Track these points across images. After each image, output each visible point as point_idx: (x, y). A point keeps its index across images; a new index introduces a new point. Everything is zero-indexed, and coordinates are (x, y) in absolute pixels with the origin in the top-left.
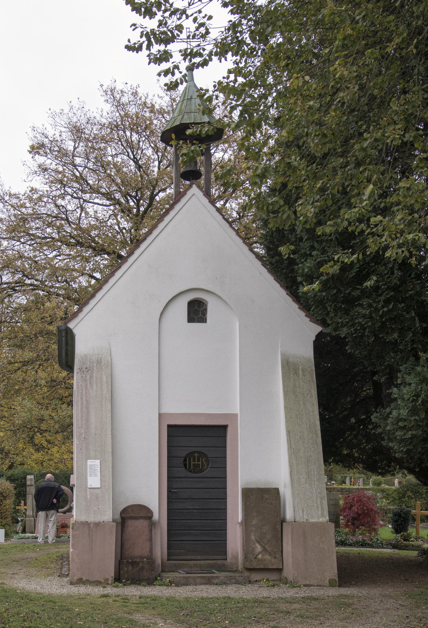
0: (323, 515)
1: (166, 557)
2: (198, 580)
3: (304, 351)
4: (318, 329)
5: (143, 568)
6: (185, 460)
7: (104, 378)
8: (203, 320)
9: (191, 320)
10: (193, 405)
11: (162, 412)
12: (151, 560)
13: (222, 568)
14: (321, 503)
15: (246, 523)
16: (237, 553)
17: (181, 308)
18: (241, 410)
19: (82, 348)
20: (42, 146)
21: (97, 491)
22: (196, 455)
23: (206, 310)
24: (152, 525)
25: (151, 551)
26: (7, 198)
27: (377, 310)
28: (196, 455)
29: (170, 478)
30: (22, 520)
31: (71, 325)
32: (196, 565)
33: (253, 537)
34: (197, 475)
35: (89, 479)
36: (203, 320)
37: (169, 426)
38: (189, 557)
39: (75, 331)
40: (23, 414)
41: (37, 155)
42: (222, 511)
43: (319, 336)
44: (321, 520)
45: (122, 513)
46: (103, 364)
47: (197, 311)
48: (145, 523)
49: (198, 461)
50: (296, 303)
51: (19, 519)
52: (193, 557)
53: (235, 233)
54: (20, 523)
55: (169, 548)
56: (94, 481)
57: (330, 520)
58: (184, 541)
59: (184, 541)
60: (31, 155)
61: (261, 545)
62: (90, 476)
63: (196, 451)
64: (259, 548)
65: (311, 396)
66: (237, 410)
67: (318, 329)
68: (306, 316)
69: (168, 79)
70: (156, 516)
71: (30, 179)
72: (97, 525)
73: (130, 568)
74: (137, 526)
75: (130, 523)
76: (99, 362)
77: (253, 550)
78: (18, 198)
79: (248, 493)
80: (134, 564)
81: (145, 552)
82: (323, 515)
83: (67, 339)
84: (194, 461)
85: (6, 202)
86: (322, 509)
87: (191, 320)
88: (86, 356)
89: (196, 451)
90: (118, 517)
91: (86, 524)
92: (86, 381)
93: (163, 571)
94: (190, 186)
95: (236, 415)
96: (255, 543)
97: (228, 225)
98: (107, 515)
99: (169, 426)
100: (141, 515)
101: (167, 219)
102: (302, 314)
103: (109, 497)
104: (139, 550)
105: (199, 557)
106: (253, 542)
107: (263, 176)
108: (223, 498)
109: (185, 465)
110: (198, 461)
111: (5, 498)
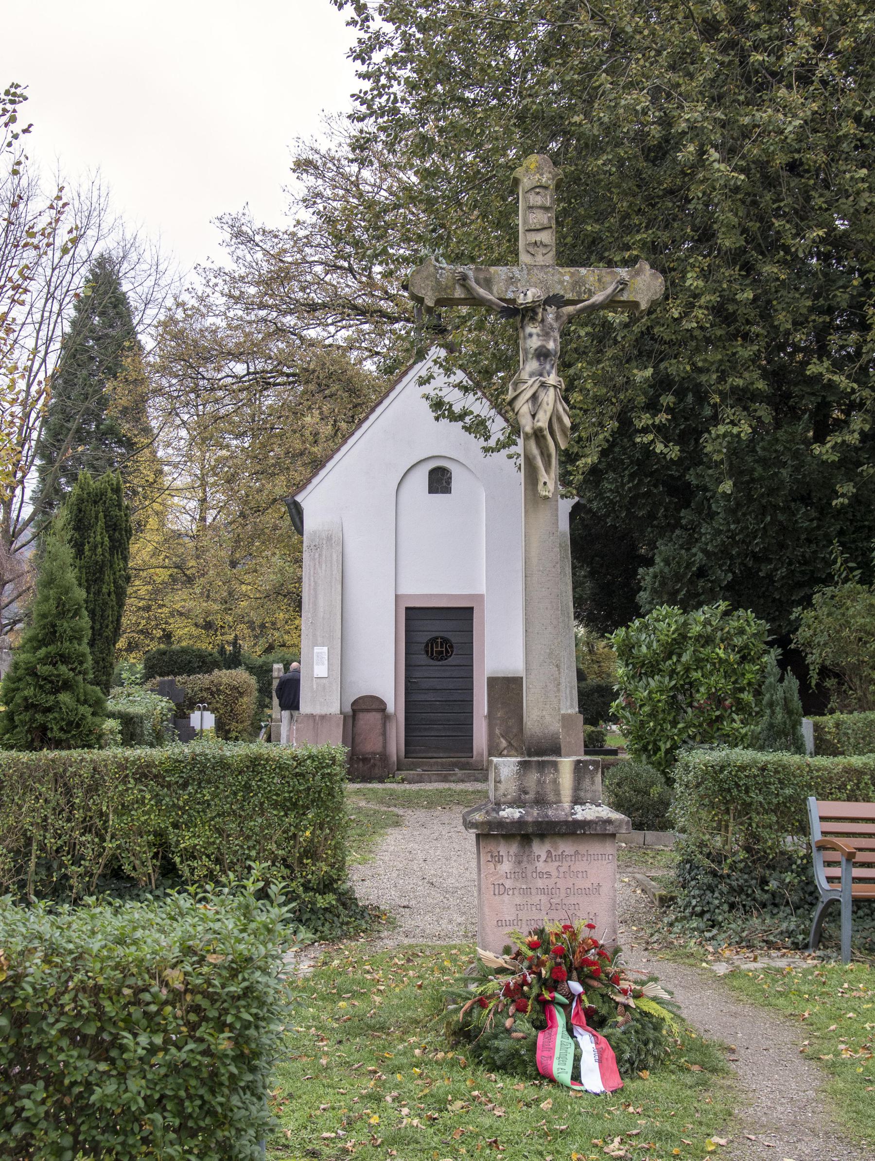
0: (572, 706)
1: (402, 753)
2: (434, 778)
5: (374, 765)
6: (427, 646)
7: (335, 556)
8: (447, 490)
9: (432, 490)
10: (434, 586)
11: (399, 593)
12: (384, 757)
13: (463, 767)
14: (571, 693)
15: (490, 716)
17: (421, 478)
18: (487, 590)
19: (310, 523)
20: (309, 163)
21: (324, 681)
23: (450, 478)
24: (386, 718)
25: (385, 746)
26: (258, 238)
27: (623, 485)
29: (408, 666)
30: (266, 726)
31: (298, 498)
32: (437, 763)
33: (497, 731)
34: (440, 663)
35: (315, 667)
36: (447, 490)
37: (407, 608)
38: (430, 755)
39: (303, 505)
40: (272, 577)
41: (305, 175)
42: (468, 702)
44: (569, 711)
45: (353, 704)
46: (335, 541)
47: (440, 480)
48: (378, 716)
51: (263, 724)
52: (435, 755)
54: (263, 730)
55: (406, 745)
56: (320, 670)
57: (580, 712)
60: (296, 175)
62: (317, 665)
63: (438, 637)
65: (565, 575)
66: (482, 589)
70: (391, 708)
71: (294, 210)
72: (323, 717)
73: (361, 764)
74: (369, 719)
75: (361, 715)
76: (329, 539)
77: (498, 745)
78: (276, 236)
79: (493, 682)
80: (365, 760)
81: (378, 748)
82: (572, 706)
83: (296, 512)
85: (257, 245)
86: (572, 699)
87: (432, 490)
88: (315, 532)
89: (438, 637)
90: (348, 709)
91: (312, 716)
92: (314, 559)
93: (398, 769)
95: (482, 596)
98: (334, 708)
99: (407, 608)
100: (373, 707)
101: (379, 410)
103: (336, 687)
104: (371, 745)
105: (441, 755)
108: (469, 690)
109: (427, 652)
111: (241, 694)
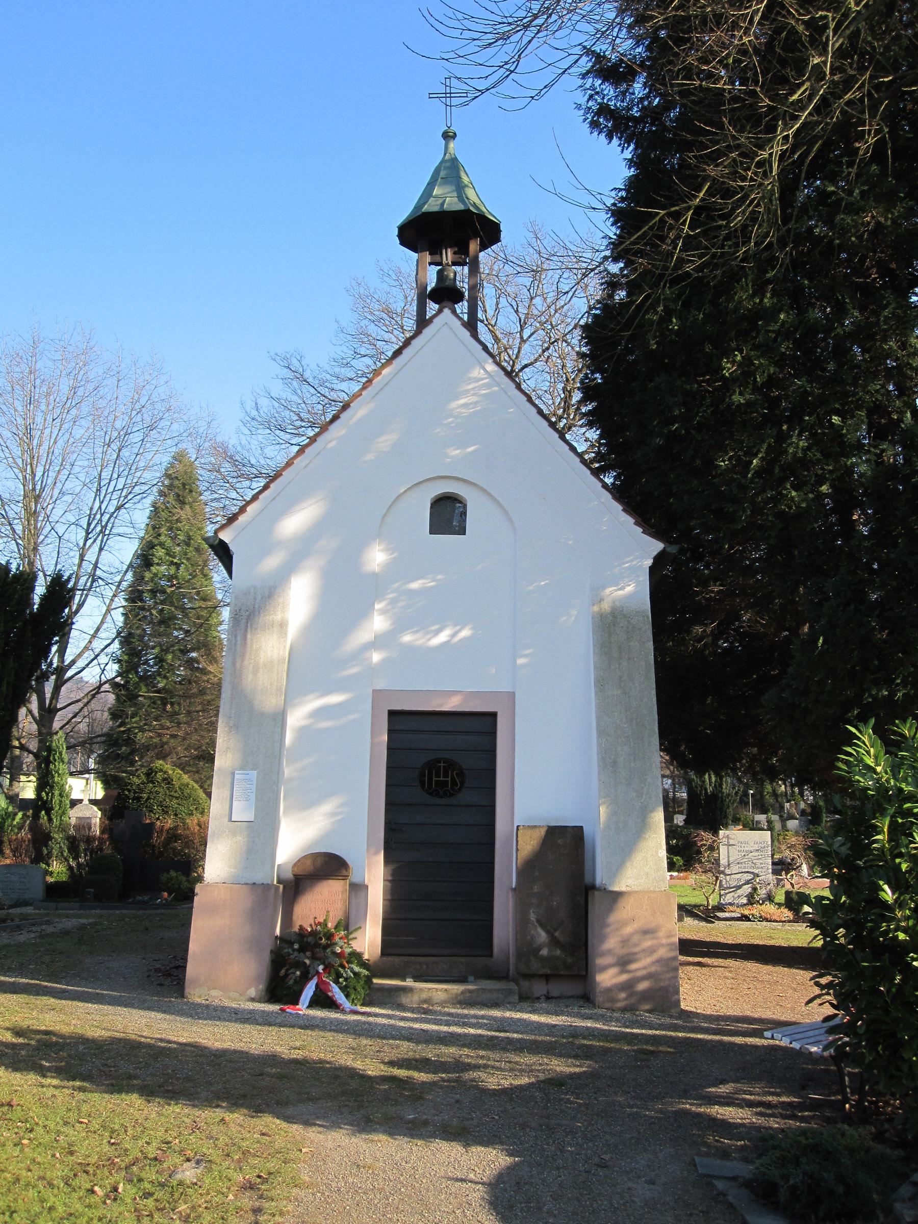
3: (631, 588)
4: (657, 546)
6: (422, 775)
16: (508, 957)
22: (442, 764)
28: (442, 764)
33: (532, 917)
43: (659, 560)
49: (446, 775)
50: (630, 515)
53: (557, 435)
58: (422, 919)
59: (422, 919)
61: (548, 932)
64: (542, 936)
67: (657, 546)
68: (635, 524)
69: (695, 930)
84: (438, 775)
89: (439, 767)
94: (440, 311)
96: (535, 927)
97: (556, 435)
102: (629, 520)
106: (533, 924)
107: (202, 736)
109: (422, 784)
110: (446, 775)
